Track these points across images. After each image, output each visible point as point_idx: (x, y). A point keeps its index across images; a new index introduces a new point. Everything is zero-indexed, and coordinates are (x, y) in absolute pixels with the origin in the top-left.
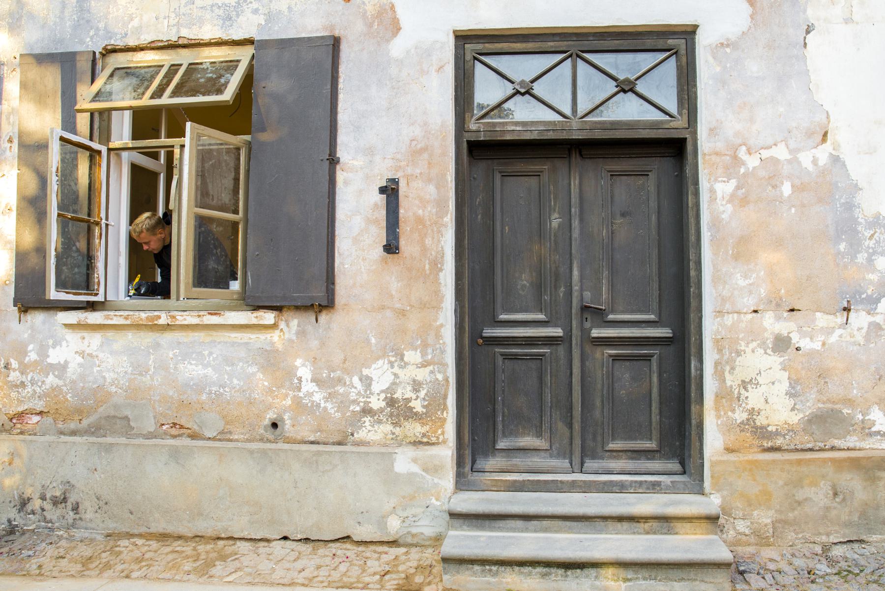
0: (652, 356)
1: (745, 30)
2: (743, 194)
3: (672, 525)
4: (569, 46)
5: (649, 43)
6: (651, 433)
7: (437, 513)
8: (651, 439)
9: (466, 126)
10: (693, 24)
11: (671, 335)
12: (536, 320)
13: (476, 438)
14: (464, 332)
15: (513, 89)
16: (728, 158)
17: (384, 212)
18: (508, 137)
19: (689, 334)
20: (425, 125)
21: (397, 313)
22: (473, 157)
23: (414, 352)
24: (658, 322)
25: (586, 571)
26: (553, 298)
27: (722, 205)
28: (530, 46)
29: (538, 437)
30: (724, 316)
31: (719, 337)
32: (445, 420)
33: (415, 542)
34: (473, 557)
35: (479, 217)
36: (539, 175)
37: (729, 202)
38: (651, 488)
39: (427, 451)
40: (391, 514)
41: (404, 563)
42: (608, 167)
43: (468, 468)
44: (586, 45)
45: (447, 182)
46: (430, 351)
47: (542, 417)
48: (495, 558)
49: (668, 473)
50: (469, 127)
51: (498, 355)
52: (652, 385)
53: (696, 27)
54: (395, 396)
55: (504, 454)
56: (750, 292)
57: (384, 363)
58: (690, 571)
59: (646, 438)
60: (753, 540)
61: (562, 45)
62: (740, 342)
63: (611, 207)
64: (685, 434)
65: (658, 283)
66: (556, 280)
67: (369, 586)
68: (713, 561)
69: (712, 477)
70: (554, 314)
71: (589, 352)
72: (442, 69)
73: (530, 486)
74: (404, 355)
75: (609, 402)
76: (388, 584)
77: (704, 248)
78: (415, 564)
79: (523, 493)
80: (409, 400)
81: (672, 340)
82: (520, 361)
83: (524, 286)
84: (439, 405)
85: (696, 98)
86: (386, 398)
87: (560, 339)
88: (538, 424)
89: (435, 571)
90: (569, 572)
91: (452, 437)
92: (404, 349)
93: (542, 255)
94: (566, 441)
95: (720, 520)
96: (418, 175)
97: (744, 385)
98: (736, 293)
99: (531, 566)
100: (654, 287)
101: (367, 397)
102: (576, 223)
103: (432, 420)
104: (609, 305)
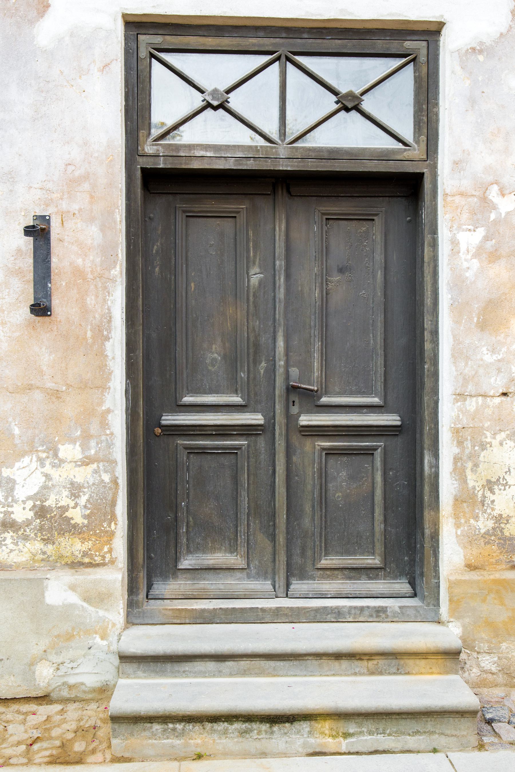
0: (376, 450)
1: (504, 30)
2: (492, 246)
3: (402, 662)
4: (273, 44)
5: (380, 45)
6: (374, 546)
7: (102, 656)
8: (373, 554)
9: (139, 148)
10: (438, 20)
11: (399, 423)
12: (231, 403)
13: (153, 555)
14: (138, 420)
15: (203, 101)
16: (476, 199)
17: (30, 260)
18: (196, 165)
19: (422, 421)
20: (85, 144)
21: (48, 394)
22: (149, 191)
23: (71, 446)
24: (382, 407)
25: (297, 725)
26: (252, 376)
27: (466, 260)
28: (225, 42)
29: (231, 552)
30: (465, 400)
31: (460, 426)
32: (112, 534)
33: (72, 696)
34: (151, 713)
35: (157, 269)
36: (235, 217)
37: (475, 256)
38: (374, 615)
39: (90, 574)
40: (41, 660)
41: (59, 726)
42: (323, 209)
43: (142, 595)
44: (299, 44)
45: (115, 222)
46: (93, 443)
47: (237, 527)
48: (181, 713)
49: (395, 596)
50: (143, 150)
51: (180, 448)
52: (375, 485)
53: (441, 24)
54: (47, 504)
55: (188, 575)
56: (499, 370)
57: (31, 461)
58: (427, 721)
59: (368, 552)
60: (501, 679)
61: (267, 43)
62: (485, 432)
63: (326, 261)
64: (415, 547)
65: (383, 357)
66: (255, 353)
67: (12, 761)
68: (455, 709)
69: (451, 601)
70: (253, 396)
71: (297, 444)
72: (107, 68)
73: (222, 617)
74: (59, 449)
75: (321, 508)
76: (36, 756)
77: (443, 313)
78: (73, 726)
79: (214, 625)
80: (65, 509)
81: (400, 429)
82: (209, 457)
83: (214, 360)
84: (105, 514)
85: (437, 121)
86: (34, 506)
87: (259, 428)
88: (232, 536)
89: (101, 733)
90: (276, 728)
91: (122, 555)
92: (59, 441)
93: (239, 321)
94: (268, 557)
95: (461, 654)
96: (77, 212)
97: (490, 485)
98: (481, 371)
99: (227, 721)
100: (379, 363)
101: (8, 506)
102: (281, 280)
103: (95, 534)
104: (321, 385)
